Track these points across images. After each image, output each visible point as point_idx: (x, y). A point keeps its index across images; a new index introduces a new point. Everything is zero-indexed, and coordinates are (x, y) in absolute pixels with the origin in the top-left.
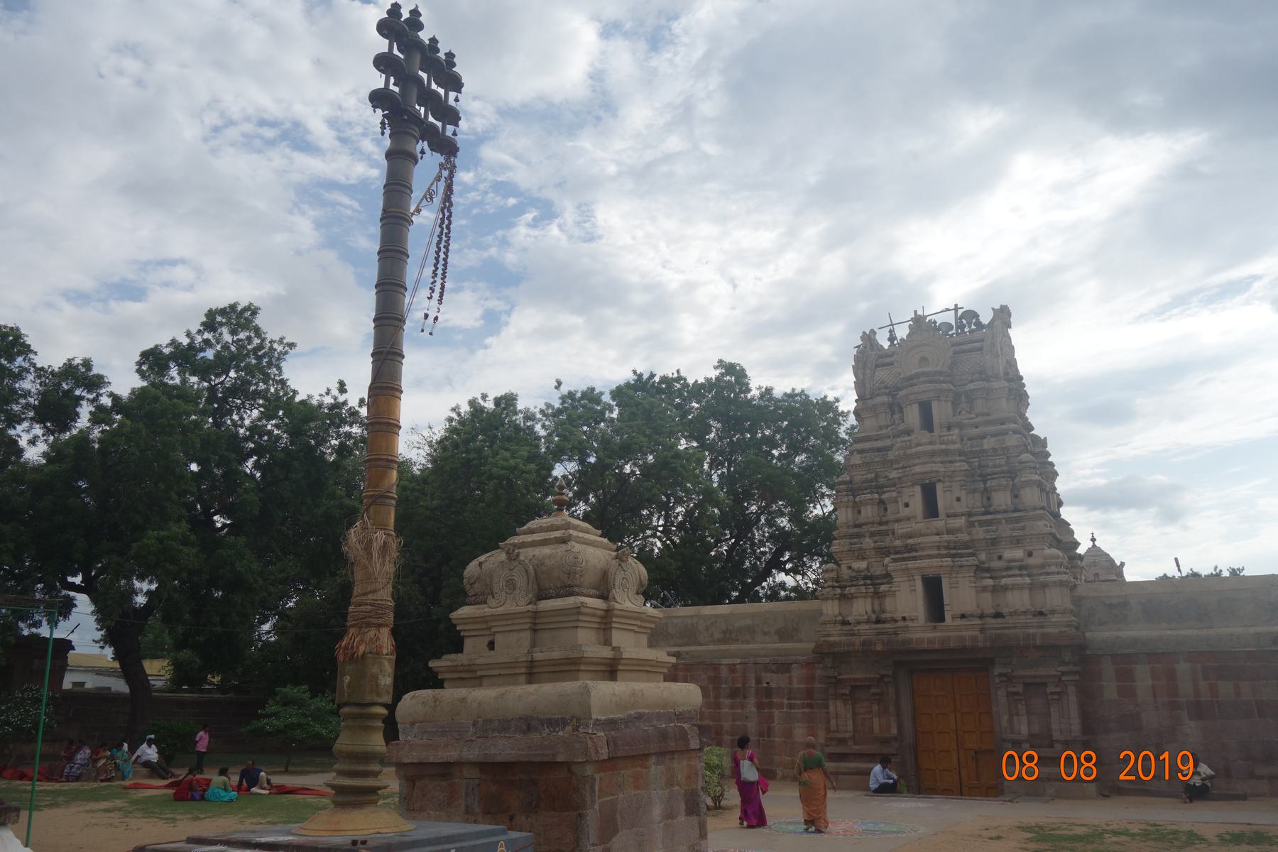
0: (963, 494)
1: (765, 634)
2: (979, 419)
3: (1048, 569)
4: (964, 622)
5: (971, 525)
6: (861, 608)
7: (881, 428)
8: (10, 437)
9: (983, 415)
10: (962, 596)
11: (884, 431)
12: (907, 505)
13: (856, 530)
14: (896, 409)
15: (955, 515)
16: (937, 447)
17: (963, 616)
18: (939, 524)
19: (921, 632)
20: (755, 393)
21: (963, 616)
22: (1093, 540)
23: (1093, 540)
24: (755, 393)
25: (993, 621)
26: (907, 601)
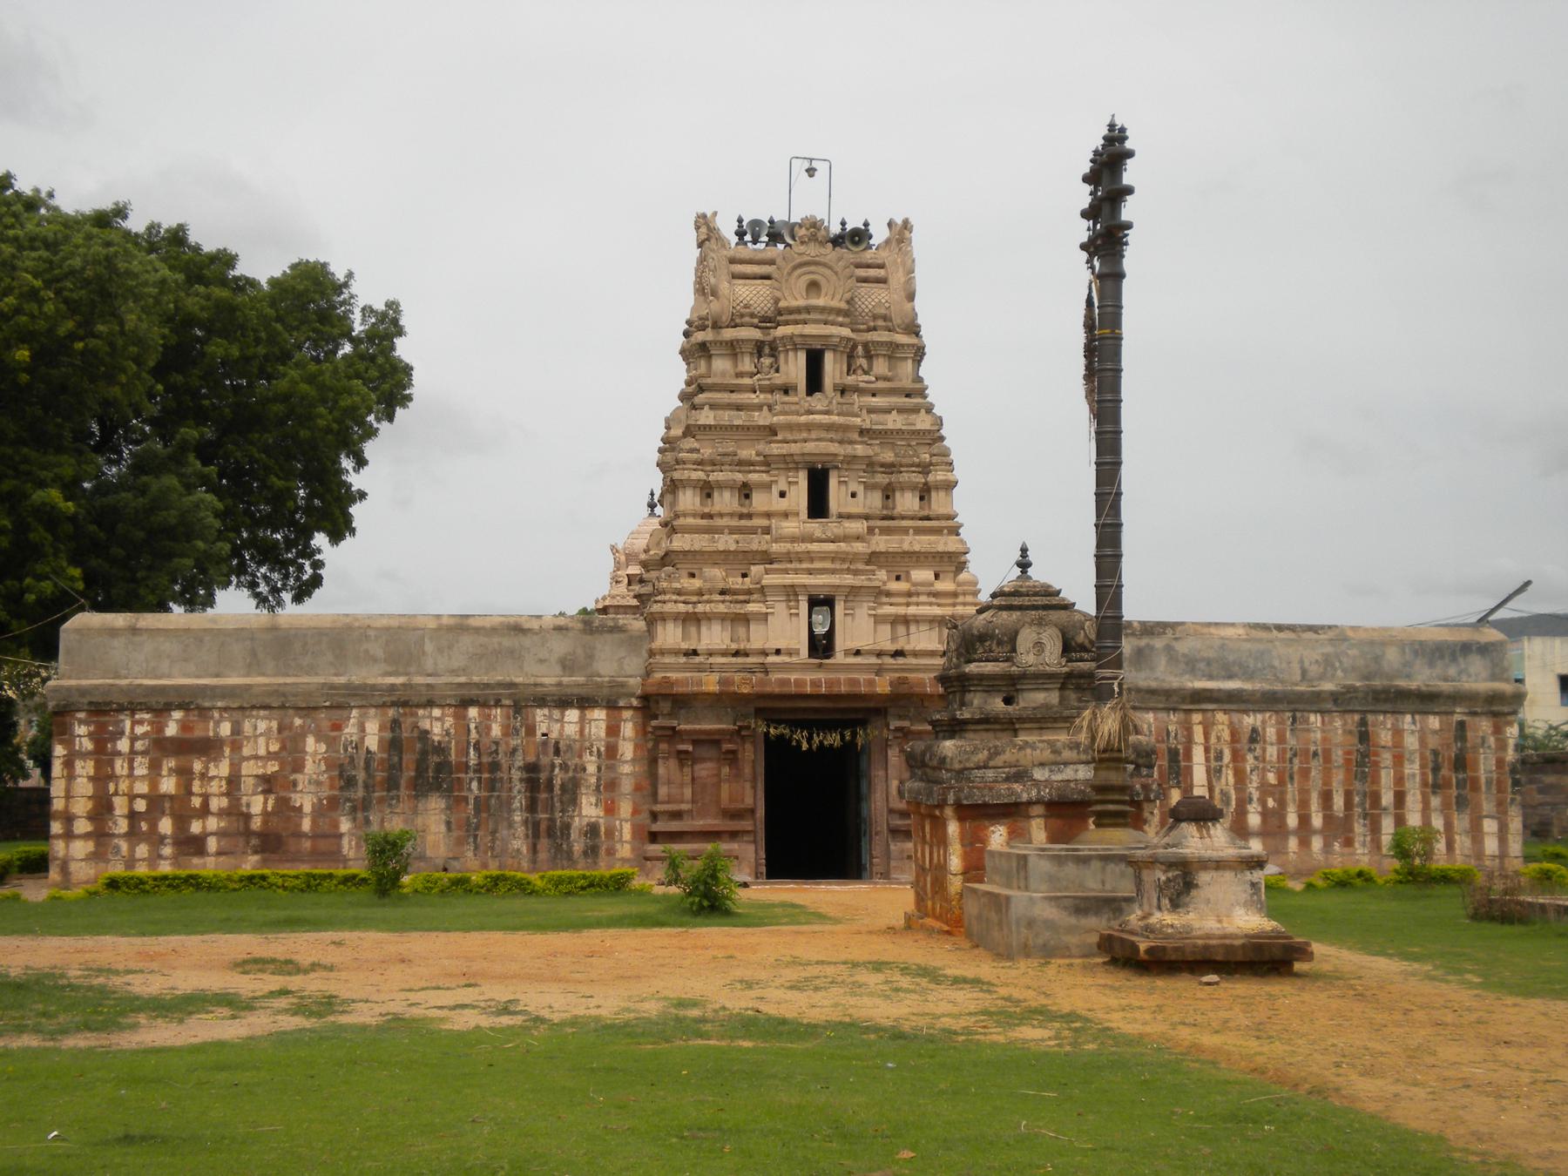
0: (860, 490)
1: (541, 661)
2: (881, 385)
3: (961, 599)
4: (858, 660)
5: (871, 530)
6: (714, 637)
7: (739, 375)
8: (337, 462)
9: (886, 379)
10: (857, 630)
11: (747, 381)
12: (782, 495)
13: (704, 522)
14: (767, 350)
15: (849, 517)
16: (835, 418)
17: (858, 653)
18: (831, 527)
19: (808, 678)
20: (265, 286)
21: (858, 653)
22: (1024, 565)
23: (1024, 565)
24: (265, 286)
25: (891, 661)
26: (786, 630)
